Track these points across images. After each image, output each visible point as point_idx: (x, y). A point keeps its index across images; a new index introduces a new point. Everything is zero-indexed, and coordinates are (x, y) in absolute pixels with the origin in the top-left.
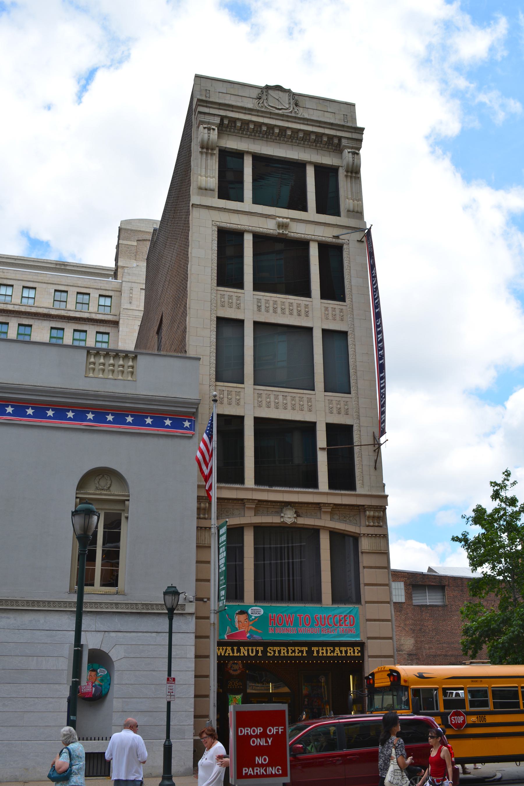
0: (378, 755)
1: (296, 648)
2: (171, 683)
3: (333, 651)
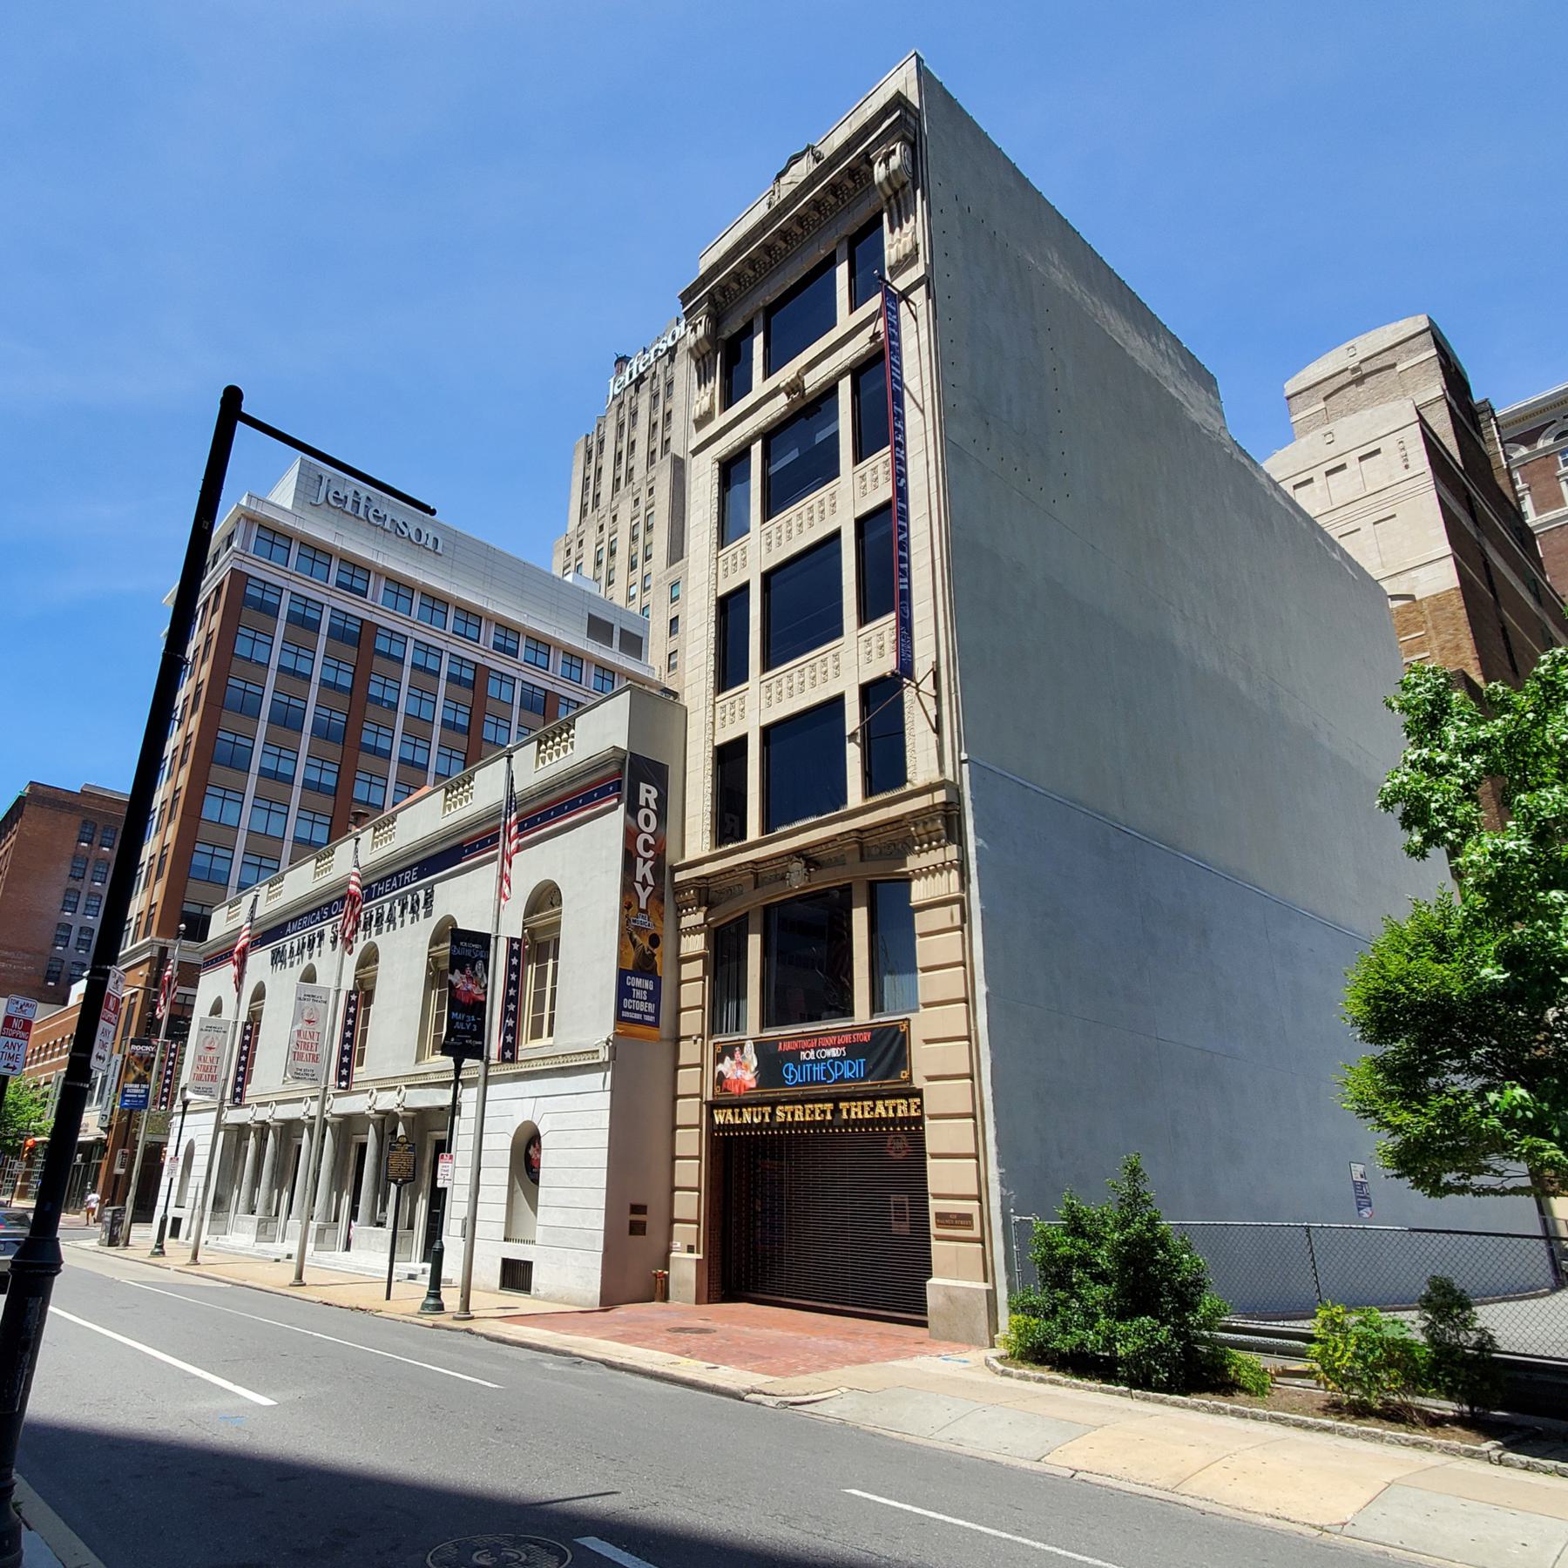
0: (1484, 677)
1: (817, 1106)
2: (14, 1037)
3: (873, 1109)
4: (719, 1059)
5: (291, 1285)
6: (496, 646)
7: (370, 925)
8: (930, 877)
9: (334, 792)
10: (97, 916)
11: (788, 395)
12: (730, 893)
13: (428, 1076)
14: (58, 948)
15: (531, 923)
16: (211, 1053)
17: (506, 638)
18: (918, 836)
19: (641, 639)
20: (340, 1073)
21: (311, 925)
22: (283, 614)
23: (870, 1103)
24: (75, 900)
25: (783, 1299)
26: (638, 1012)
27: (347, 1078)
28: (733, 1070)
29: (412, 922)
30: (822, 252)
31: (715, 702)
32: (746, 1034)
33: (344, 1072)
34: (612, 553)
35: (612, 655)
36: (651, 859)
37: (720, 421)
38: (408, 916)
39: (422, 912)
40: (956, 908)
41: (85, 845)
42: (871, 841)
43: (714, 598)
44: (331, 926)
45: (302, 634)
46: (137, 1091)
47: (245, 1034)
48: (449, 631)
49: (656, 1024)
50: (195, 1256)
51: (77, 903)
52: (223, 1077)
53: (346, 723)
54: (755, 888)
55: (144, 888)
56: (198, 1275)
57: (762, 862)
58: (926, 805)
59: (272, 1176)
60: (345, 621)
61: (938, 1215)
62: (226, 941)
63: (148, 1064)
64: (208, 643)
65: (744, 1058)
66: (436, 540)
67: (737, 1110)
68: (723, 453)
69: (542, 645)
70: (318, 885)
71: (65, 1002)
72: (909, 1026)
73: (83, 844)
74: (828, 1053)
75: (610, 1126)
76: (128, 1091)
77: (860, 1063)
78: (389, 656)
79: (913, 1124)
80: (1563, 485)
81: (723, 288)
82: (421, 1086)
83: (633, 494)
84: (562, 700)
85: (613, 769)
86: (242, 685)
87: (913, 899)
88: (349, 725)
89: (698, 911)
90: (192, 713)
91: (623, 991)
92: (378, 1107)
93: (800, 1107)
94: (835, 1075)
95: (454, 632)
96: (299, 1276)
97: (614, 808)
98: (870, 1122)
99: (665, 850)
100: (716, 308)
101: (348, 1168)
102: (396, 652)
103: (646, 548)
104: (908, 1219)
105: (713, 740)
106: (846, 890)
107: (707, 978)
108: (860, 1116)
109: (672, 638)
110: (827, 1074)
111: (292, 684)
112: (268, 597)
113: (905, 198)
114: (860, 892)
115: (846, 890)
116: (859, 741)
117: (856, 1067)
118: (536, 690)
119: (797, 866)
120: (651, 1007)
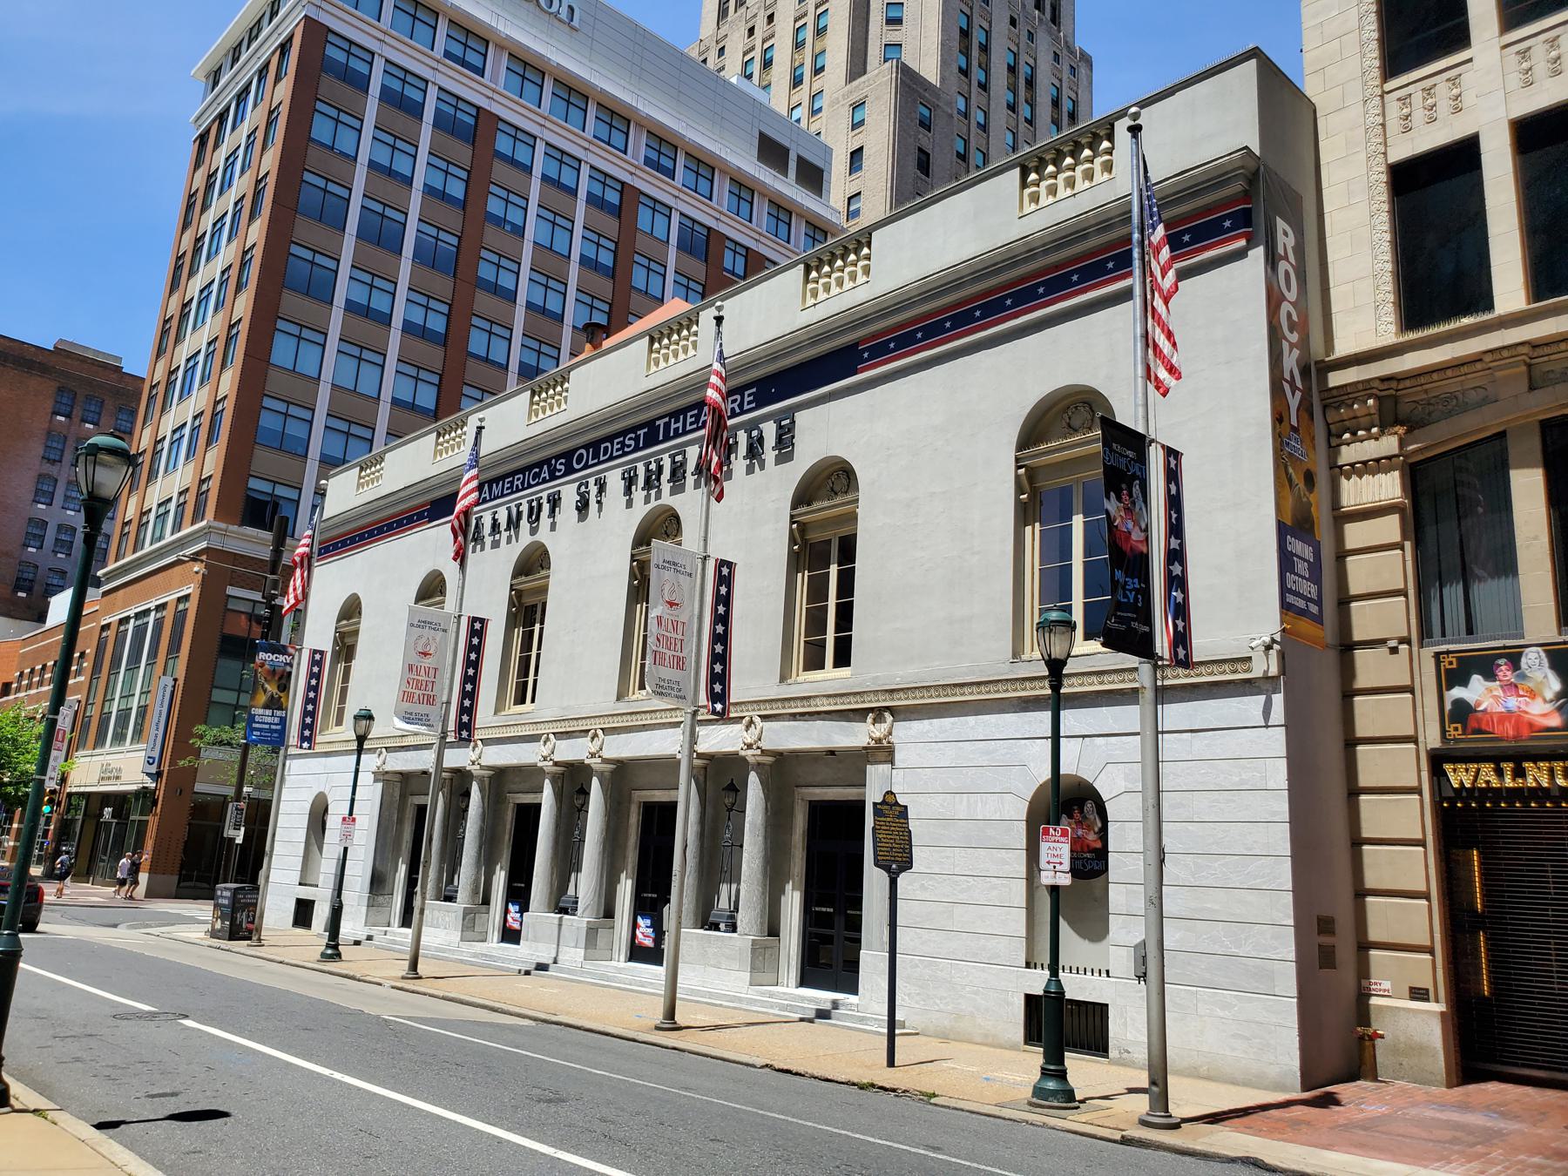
5: (658, 1028)
6: (648, 161)
7: (658, 479)
9: (444, 340)
10: (79, 511)
12: (1454, 406)
13: (812, 702)
14: (30, 549)
15: (800, 515)
16: (428, 662)
17: (659, 152)
19: (822, 171)
20: (302, 734)
21: (530, 486)
22: (375, 89)
24: (51, 489)
26: (267, 723)
27: (309, 739)
28: (1496, 697)
29: (750, 470)
33: (307, 733)
34: (767, 64)
35: (788, 187)
38: (739, 463)
39: (770, 455)
41: (63, 419)
44: (620, 470)
45: (400, 121)
46: (269, 720)
47: (472, 637)
48: (589, 134)
49: (1318, 619)
50: (414, 965)
51: (53, 494)
52: (445, 699)
53: (458, 248)
54: (1532, 388)
55: (187, 458)
56: (444, 998)
57: (1547, 344)
59: (480, 847)
60: (456, 108)
62: (442, 486)
63: (283, 681)
64: (270, 123)
65: (1524, 677)
66: (571, 9)
69: (704, 167)
70: (538, 429)
71: (42, 618)
73: (59, 418)
75: (1289, 785)
76: (257, 719)
78: (513, 162)
82: (794, 717)
83: (766, 9)
84: (728, 243)
85: (1237, 187)
86: (321, 183)
88: (462, 250)
89: (1382, 433)
90: (252, 218)
91: (1286, 561)
92: (557, 758)
95: (595, 137)
96: (670, 1013)
97: (1240, 255)
101: (626, 839)
102: (522, 155)
103: (816, 57)
105: (1385, 154)
109: (854, 176)
111: (389, 189)
112: (355, 64)
118: (697, 227)
120: (1314, 589)
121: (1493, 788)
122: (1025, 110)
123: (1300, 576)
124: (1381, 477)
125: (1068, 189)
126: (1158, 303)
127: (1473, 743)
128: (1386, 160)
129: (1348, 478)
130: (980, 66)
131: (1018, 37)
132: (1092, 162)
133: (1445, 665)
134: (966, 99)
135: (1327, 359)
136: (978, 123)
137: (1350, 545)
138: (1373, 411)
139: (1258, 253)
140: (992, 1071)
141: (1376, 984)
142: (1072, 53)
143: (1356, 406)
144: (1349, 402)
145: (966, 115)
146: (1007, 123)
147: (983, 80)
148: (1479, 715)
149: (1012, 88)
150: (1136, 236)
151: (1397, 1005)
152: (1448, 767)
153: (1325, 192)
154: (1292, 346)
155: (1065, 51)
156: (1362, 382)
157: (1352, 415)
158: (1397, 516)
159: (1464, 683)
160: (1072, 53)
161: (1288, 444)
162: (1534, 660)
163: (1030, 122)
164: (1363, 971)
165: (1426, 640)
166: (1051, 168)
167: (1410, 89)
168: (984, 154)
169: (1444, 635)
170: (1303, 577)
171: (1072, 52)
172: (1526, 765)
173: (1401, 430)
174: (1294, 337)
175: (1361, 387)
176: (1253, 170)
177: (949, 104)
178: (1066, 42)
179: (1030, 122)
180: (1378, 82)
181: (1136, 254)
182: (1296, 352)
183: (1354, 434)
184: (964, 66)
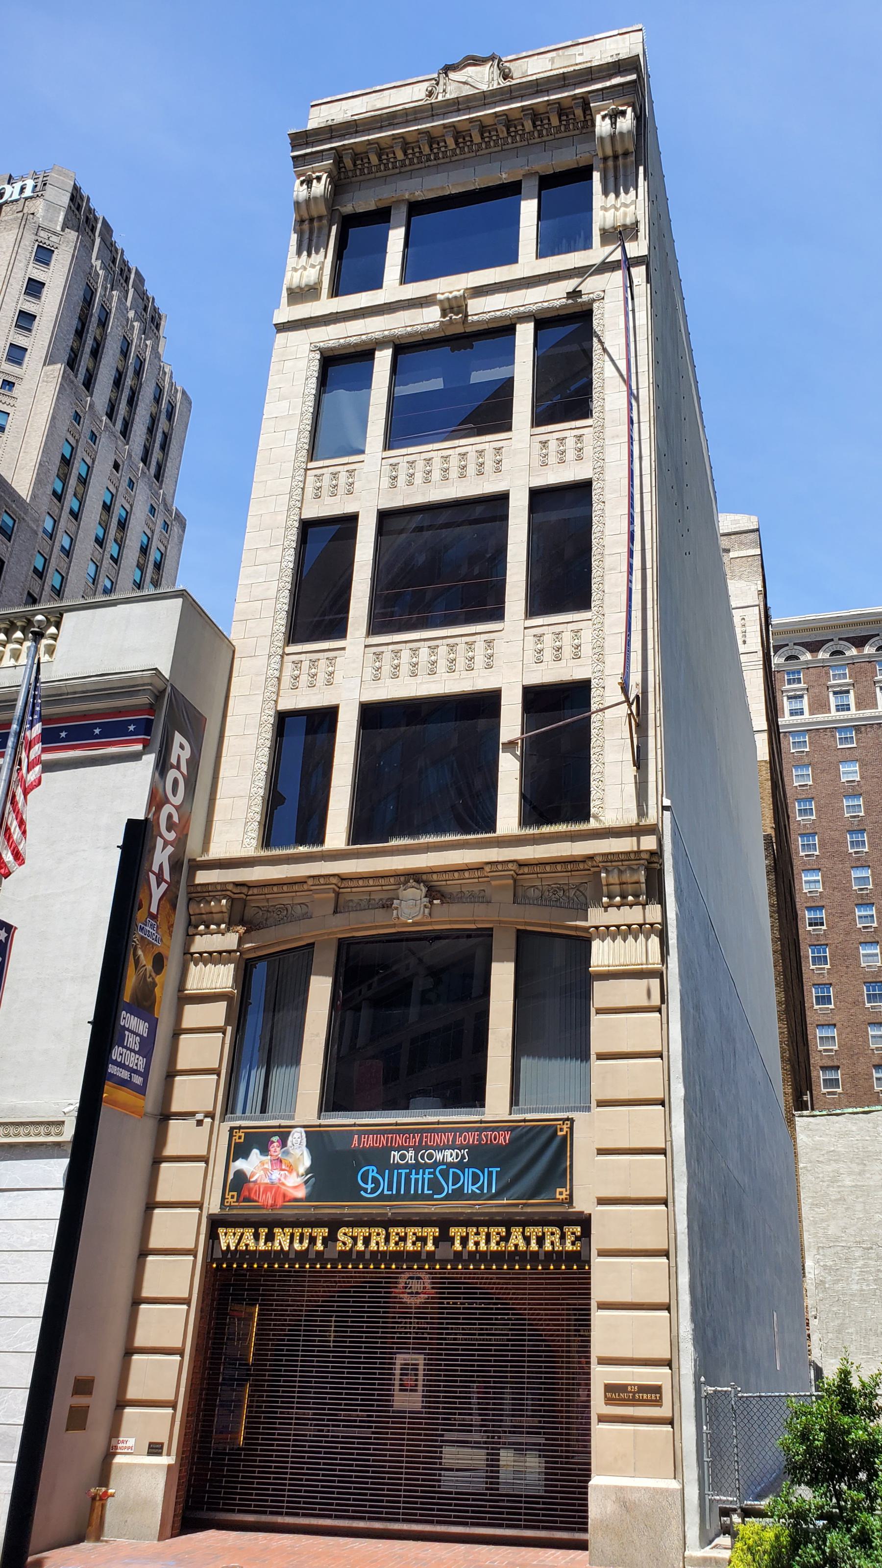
1: (411, 1231)
3: (506, 1239)
4: (239, 1151)
8: (619, 939)
11: (444, 314)
18: (607, 885)
23: (503, 1230)
25: (280, 1519)
28: (265, 1170)
30: (504, 176)
31: (284, 653)
32: (292, 1118)
36: (171, 843)
37: (326, 305)
40: (655, 983)
42: (529, 879)
43: (297, 518)
49: (141, 1090)
54: (335, 912)
58: (628, 849)
61: (609, 1388)
65: (287, 1153)
67: (263, 1231)
68: (331, 344)
72: (571, 1128)
74: (439, 1156)
77: (490, 1174)
79: (406, 1261)
80: (878, 689)
81: (358, 155)
85: (144, 700)
87: (594, 961)
93: (382, 1231)
94: (448, 1188)
97: (135, 757)
98: (498, 1257)
99: (187, 835)
100: (339, 173)
104: (420, 1388)
105: (276, 702)
106: (487, 934)
107: (229, 1029)
108: (483, 1247)
110: (435, 1186)
113: (625, 167)
114: (504, 942)
115: (487, 934)
116: (519, 753)
117: (484, 1179)
119: (414, 894)
120: (141, 1062)
121: (250, 1251)
122: (112, 548)
123: (128, 1049)
124: (221, 967)
125: (47, 655)
126: (19, 792)
127: (244, 1211)
128: (276, 707)
129: (196, 965)
130: (75, 495)
131: (119, 481)
132: (21, 644)
133: (236, 1139)
134: (55, 521)
135: (198, 859)
136: (62, 547)
137: (186, 1024)
138: (224, 910)
139: (150, 759)
140: (131, 1544)
141: (123, 1442)
142: (168, 510)
143: (213, 903)
144: (208, 898)
145: (51, 536)
146: (92, 555)
147: (76, 509)
148: (251, 1185)
149: (104, 525)
150: (15, 727)
151: (135, 1462)
152: (221, 1231)
153: (229, 719)
154: (166, 843)
155: (161, 507)
156: (221, 883)
157: (208, 910)
158: (226, 1003)
159: (246, 1155)
160: (168, 510)
161: (142, 929)
162: (297, 1138)
163: (116, 560)
164: (115, 1430)
165: (228, 1115)
166: (19, 635)
167: (303, 657)
168: (63, 577)
169: (244, 1112)
170: (132, 1050)
171: (168, 510)
172: (276, 1230)
173: (241, 929)
174: (171, 836)
175: (219, 888)
176: (161, 689)
177: (36, 521)
178: (164, 499)
179: (116, 560)
180: (281, 644)
181: (10, 742)
182: (170, 849)
183: (207, 927)
184: (59, 491)
